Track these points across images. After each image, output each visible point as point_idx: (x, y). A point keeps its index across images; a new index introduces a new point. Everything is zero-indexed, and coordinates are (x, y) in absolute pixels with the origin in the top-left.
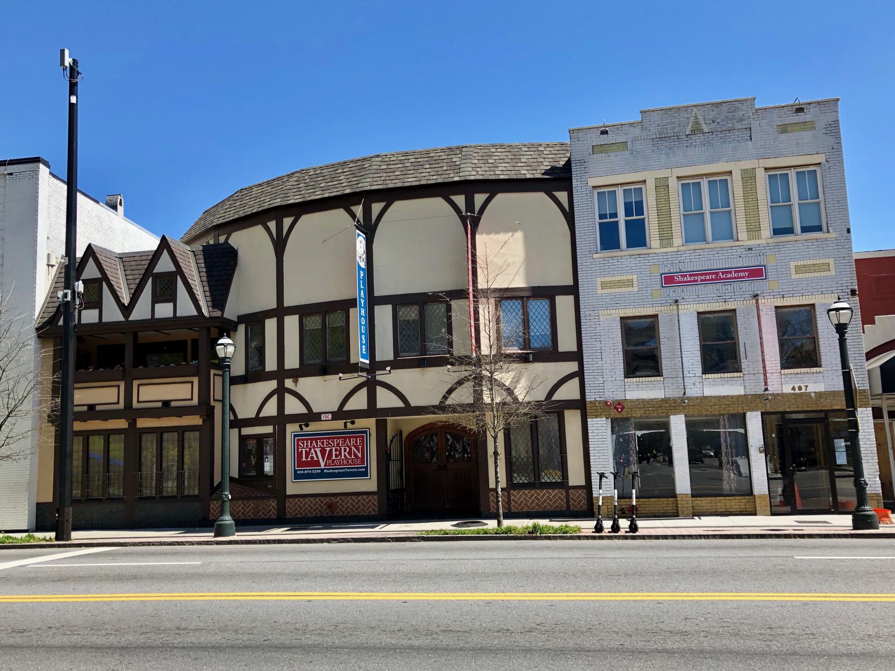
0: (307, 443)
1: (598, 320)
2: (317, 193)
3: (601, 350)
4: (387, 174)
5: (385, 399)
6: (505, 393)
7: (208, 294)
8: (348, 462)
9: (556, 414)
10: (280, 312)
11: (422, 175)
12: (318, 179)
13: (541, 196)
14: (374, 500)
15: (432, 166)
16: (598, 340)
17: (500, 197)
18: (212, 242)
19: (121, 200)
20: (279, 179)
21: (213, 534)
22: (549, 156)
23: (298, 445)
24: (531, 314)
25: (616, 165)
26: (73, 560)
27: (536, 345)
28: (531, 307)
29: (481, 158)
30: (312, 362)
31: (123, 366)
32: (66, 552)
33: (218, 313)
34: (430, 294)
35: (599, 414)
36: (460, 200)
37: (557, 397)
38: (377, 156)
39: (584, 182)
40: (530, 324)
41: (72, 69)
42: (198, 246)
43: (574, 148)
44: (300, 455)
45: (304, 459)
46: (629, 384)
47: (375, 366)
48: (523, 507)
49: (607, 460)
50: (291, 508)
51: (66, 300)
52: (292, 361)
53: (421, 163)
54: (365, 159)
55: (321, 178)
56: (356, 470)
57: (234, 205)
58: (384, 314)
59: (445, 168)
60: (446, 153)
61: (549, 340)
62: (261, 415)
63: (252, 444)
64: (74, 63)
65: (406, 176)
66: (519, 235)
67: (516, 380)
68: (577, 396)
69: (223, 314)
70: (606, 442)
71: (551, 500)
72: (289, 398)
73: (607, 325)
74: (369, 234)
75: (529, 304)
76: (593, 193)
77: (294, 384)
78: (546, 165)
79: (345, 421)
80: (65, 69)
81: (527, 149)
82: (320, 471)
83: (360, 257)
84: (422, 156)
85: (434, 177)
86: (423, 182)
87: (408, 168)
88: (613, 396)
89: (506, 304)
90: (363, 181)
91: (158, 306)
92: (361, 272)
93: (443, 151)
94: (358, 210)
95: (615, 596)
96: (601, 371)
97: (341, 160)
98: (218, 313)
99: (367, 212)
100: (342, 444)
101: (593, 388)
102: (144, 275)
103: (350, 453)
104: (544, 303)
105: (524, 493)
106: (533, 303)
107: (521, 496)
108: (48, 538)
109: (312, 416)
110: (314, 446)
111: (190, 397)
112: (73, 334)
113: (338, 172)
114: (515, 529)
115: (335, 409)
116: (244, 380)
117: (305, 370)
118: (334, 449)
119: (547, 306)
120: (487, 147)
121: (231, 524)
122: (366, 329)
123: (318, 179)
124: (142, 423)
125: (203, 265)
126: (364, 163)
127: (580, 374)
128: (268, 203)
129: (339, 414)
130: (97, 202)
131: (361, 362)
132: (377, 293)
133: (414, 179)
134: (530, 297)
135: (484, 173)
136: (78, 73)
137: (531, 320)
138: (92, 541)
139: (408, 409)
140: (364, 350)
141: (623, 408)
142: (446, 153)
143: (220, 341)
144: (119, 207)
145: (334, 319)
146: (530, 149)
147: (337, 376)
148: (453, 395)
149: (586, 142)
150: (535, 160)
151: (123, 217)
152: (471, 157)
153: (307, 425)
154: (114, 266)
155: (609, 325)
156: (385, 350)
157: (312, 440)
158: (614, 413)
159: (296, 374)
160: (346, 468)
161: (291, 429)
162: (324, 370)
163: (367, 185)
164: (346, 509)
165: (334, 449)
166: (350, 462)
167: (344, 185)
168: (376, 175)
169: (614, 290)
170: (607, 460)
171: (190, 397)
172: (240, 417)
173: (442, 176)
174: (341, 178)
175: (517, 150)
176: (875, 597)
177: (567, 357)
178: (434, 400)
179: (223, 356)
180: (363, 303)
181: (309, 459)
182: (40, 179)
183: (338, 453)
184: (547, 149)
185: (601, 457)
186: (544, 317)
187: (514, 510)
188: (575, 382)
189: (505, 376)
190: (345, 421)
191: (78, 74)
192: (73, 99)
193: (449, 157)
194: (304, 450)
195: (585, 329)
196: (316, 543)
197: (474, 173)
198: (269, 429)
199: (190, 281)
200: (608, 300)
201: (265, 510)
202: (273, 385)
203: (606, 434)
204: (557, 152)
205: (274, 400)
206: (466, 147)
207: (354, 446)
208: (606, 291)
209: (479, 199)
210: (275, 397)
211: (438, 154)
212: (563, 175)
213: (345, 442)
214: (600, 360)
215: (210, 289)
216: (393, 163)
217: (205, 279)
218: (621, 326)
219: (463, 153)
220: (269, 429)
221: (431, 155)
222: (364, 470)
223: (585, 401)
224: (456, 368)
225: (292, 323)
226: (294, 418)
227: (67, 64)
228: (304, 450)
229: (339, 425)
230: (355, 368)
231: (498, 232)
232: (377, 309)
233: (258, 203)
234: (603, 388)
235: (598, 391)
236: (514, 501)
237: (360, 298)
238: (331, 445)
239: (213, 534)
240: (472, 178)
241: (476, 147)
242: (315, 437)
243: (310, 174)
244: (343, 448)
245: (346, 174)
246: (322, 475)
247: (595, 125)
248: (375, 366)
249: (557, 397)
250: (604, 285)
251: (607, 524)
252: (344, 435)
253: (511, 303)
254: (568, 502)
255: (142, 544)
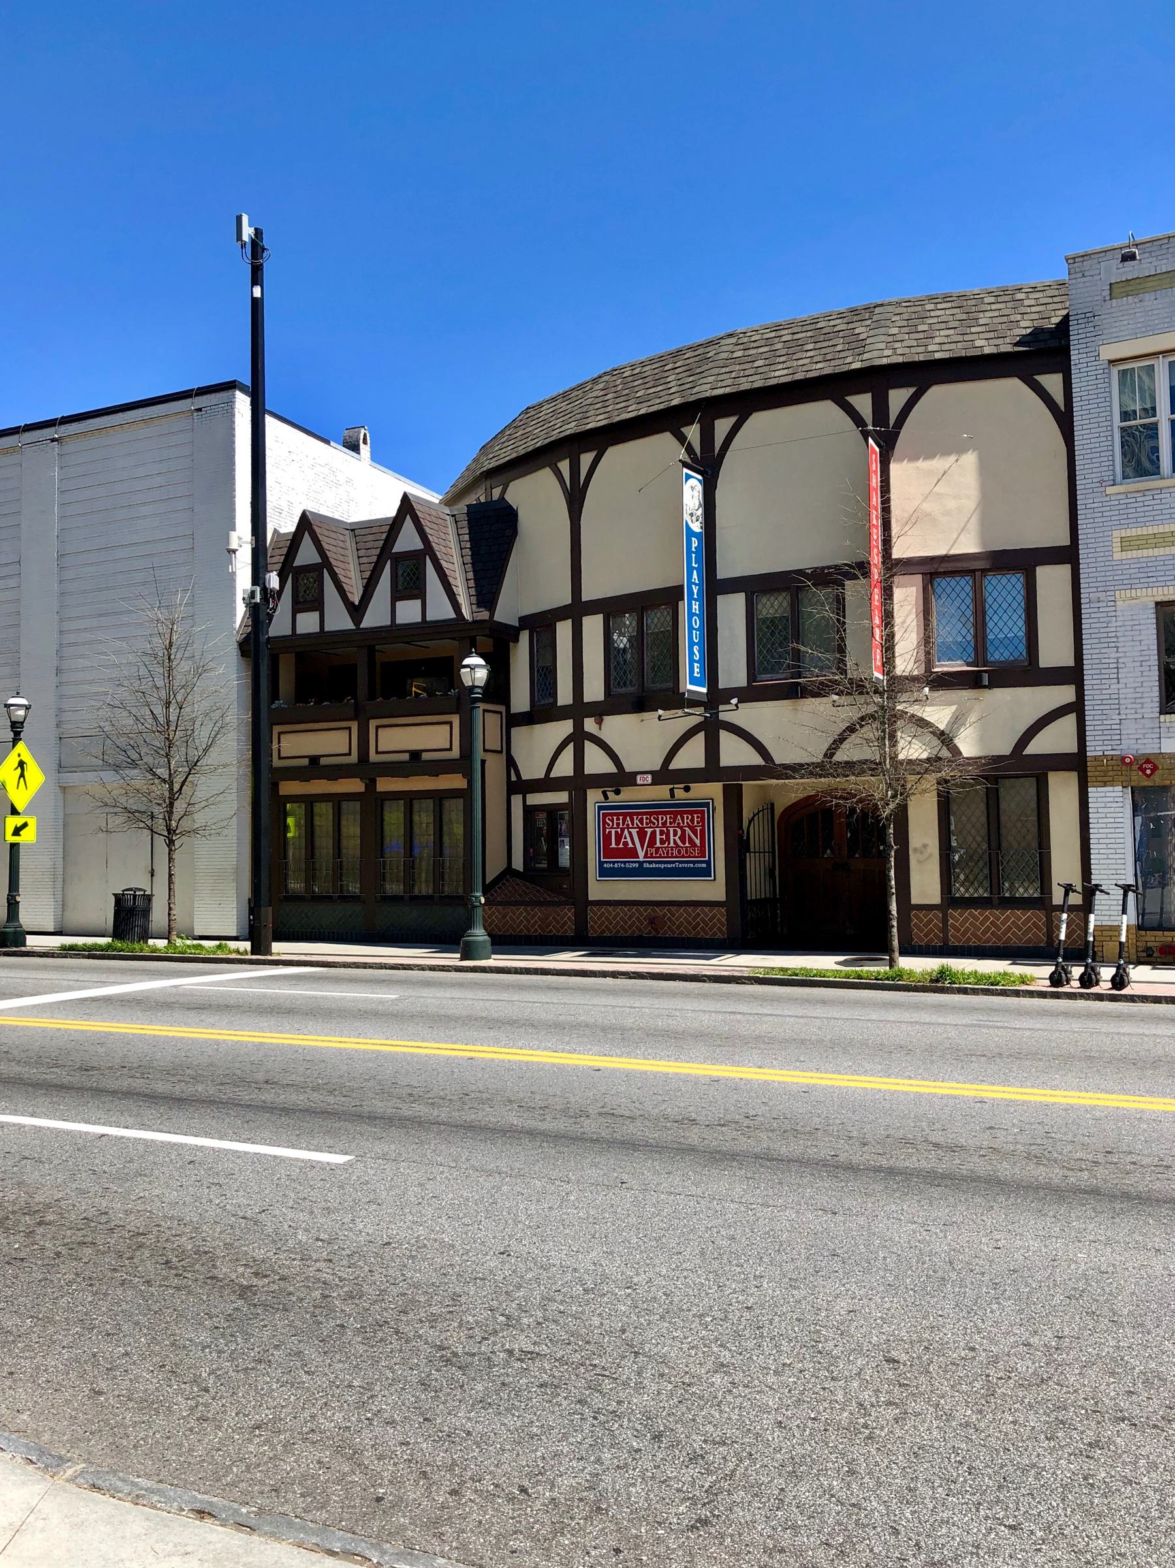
0: (618, 819)
1: (1114, 609)
2: (630, 409)
3: (1117, 662)
4: (742, 367)
5: (734, 752)
6: (936, 742)
7: (472, 583)
8: (679, 852)
9: (1033, 780)
10: (577, 610)
11: (801, 362)
12: (636, 383)
13: (1014, 385)
14: (721, 914)
15: (819, 345)
16: (1113, 645)
17: (936, 393)
18: (483, 500)
19: (365, 435)
20: (580, 387)
21: (458, 955)
22: (1033, 309)
23: (605, 822)
24: (990, 600)
25: (1154, 317)
26: (244, 984)
27: (997, 656)
28: (990, 588)
29: (905, 324)
30: (623, 690)
31: (355, 697)
32: (251, 971)
33: (484, 615)
34: (809, 571)
35: (1111, 779)
36: (863, 403)
37: (1032, 748)
38: (730, 335)
39: (1092, 354)
40: (988, 618)
41: (254, 243)
42: (461, 507)
43: (1074, 292)
44: (607, 838)
45: (613, 845)
46: (1168, 725)
47: (717, 697)
48: (969, 939)
49: (1123, 861)
50: (596, 923)
51: (253, 601)
52: (594, 690)
53: (800, 342)
54: (710, 343)
55: (640, 382)
56: (692, 865)
57: (515, 436)
58: (733, 608)
59: (839, 348)
60: (845, 320)
61: (1022, 648)
62: (552, 775)
63: (542, 817)
64: (256, 235)
65: (773, 368)
66: (970, 459)
67: (958, 720)
68: (1071, 747)
69: (492, 615)
70: (1121, 830)
71: (1020, 929)
72: (590, 749)
73: (1130, 618)
74: (710, 472)
75: (987, 582)
76: (1109, 373)
77: (598, 726)
78: (1025, 327)
79: (672, 786)
80: (243, 245)
81: (992, 300)
82: (637, 865)
83: (691, 515)
84: (805, 328)
85: (820, 366)
86: (799, 376)
87: (778, 353)
88: (1139, 746)
89: (944, 583)
90: (701, 381)
91: (301, 617)
92: (693, 539)
93: (841, 317)
94: (693, 432)
95: (1030, 1094)
96: (1117, 701)
97: (673, 348)
98: (484, 615)
99: (707, 435)
100: (671, 823)
101: (1100, 733)
102: (379, 556)
103: (682, 838)
104: (1014, 580)
105: (971, 914)
106: (994, 581)
107: (966, 919)
108: (241, 950)
109: (622, 779)
110: (628, 825)
111: (347, 751)
112: (266, 652)
113: (667, 368)
114: (911, 973)
115: (657, 767)
116: (531, 718)
117: (613, 705)
118: (658, 830)
119: (1019, 586)
120: (919, 302)
121: (484, 942)
122: (701, 636)
123: (636, 383)
124: (385, 785)
125: (467, 537)
126: (707, 350)
127: (1077, 707)
128: (558, 431)
129: (663, 775)
130: (327, 442)
131: (689, 691)
132: (722, 573)
133: (785, 372)
134: (989, 570)
135: (907, 351)
136: (264, 249)
137: (990, 612)
138: (303, 958)
139: (770, 769)
140: (696, 670)
141: (1155, 769)
142: (845, 320)
143: (467, 661)
144: (362, 446)
145: (656, 620)
146: (1000, 299)
147: (655, 715)
148: (846, 745)
149: (1098, 277)
150: (1005, 319)
151: (370, 462)
152: (888, 323)
153: (617, 792)
154: (341, 544)
155: (1134, 617)
156: (733, 672)
157: (625, 815)
158: (1138, 779)
159: (599, 711)
160: (676, 862)
161: (594, 797)
162: (640, 705)
163: (706, 389)
164: (678, 927)
165: (658, 830)
166: (683, 852)
167: (672, 390)
168: (724, 370)
169: (1145, 553)
170: (1123, 861)
171: (347, 751)
172: (524, 778)
173: (833, 363)
174: (669, 379)
175: (973, 302)
176: (1022, 1094)
177: (1056, 676)
178: (814, 752)
179: (471, 684)
180: (695, 591)
181: (621, 846)
182: (236, 413)
183: (664, 837)
184: (1032, 296)
185: (1110, 856)
186: (1015, 605)
187: (953, 942)
188: (1070, 720)
189: (939, 713)
190: (672, 786)
191: (263, 252)
192: (257, 292)
193: (851, 326)
194: (613, 831)
195: (1088, 626)
196: (595, 977)
197: (889, 352)
198: (562, 797)
199: (444, 564)
200: (1133, 571)
201: (558, 922)
202: (566, 727)
203: (1121, 815)
204: (1050, 300)
205: (569, 753)
206: (882, 305)
207: (689, 826)
208: (1130, 554)
209: (897, 398)
210: (571, 746)
211: (832, 323)
212: (1053, 343)
213: (674, 822)
214: (1116, 681)
215: (475, 575)
216: (755, 345)
217: (468, 559)
218: (1157, 618)
219: (875, 318)
220: (562, 797)
221: (819, 325)
222: (704, 865)
223: (1086, 756)
224: (843, 700)
225: (593, 625)
226: (600, 781)
227: (246, 238)
228: (613, 831)
229: (661, 792)
230: (859, 687)
231: (930, 456)
232: (721, 600)
233: (545, 431)
234: (1118, 732)
235: (1109, 737)
236: (954, 927)
237: (690, 583)
238: (654, 824)
239: (458, 955)
240: (885, 361)
241: (899, 303)
242: (630, 811)
243: (624, 375)
244: (671, 830)
245: (677, 371)
246: (641, 871)
247: (1116, 245)
248: (717, 697)
249: (1032, 748)
250: (1127, 544)
251: (1107, 973)
252: (675, 809)
253: (953, 583)
254: (945, 930)
255: (357, 965)
